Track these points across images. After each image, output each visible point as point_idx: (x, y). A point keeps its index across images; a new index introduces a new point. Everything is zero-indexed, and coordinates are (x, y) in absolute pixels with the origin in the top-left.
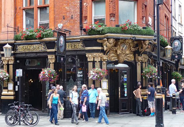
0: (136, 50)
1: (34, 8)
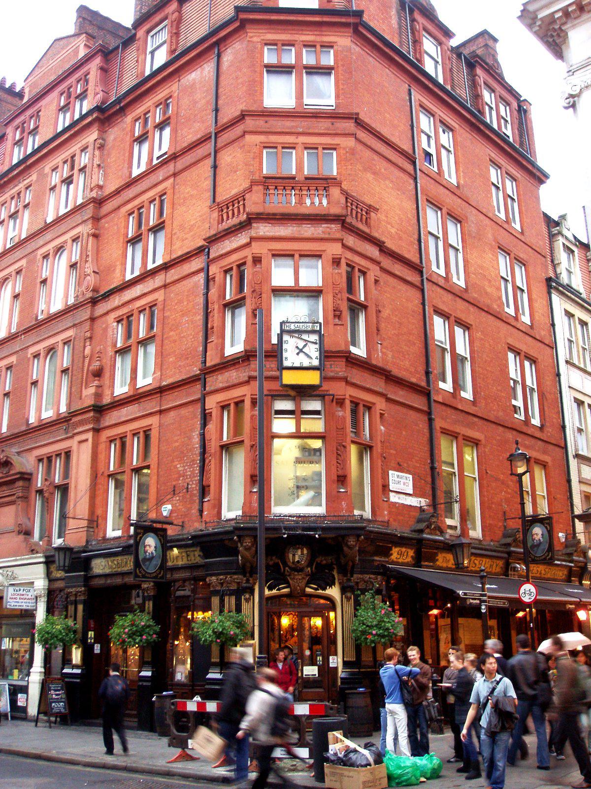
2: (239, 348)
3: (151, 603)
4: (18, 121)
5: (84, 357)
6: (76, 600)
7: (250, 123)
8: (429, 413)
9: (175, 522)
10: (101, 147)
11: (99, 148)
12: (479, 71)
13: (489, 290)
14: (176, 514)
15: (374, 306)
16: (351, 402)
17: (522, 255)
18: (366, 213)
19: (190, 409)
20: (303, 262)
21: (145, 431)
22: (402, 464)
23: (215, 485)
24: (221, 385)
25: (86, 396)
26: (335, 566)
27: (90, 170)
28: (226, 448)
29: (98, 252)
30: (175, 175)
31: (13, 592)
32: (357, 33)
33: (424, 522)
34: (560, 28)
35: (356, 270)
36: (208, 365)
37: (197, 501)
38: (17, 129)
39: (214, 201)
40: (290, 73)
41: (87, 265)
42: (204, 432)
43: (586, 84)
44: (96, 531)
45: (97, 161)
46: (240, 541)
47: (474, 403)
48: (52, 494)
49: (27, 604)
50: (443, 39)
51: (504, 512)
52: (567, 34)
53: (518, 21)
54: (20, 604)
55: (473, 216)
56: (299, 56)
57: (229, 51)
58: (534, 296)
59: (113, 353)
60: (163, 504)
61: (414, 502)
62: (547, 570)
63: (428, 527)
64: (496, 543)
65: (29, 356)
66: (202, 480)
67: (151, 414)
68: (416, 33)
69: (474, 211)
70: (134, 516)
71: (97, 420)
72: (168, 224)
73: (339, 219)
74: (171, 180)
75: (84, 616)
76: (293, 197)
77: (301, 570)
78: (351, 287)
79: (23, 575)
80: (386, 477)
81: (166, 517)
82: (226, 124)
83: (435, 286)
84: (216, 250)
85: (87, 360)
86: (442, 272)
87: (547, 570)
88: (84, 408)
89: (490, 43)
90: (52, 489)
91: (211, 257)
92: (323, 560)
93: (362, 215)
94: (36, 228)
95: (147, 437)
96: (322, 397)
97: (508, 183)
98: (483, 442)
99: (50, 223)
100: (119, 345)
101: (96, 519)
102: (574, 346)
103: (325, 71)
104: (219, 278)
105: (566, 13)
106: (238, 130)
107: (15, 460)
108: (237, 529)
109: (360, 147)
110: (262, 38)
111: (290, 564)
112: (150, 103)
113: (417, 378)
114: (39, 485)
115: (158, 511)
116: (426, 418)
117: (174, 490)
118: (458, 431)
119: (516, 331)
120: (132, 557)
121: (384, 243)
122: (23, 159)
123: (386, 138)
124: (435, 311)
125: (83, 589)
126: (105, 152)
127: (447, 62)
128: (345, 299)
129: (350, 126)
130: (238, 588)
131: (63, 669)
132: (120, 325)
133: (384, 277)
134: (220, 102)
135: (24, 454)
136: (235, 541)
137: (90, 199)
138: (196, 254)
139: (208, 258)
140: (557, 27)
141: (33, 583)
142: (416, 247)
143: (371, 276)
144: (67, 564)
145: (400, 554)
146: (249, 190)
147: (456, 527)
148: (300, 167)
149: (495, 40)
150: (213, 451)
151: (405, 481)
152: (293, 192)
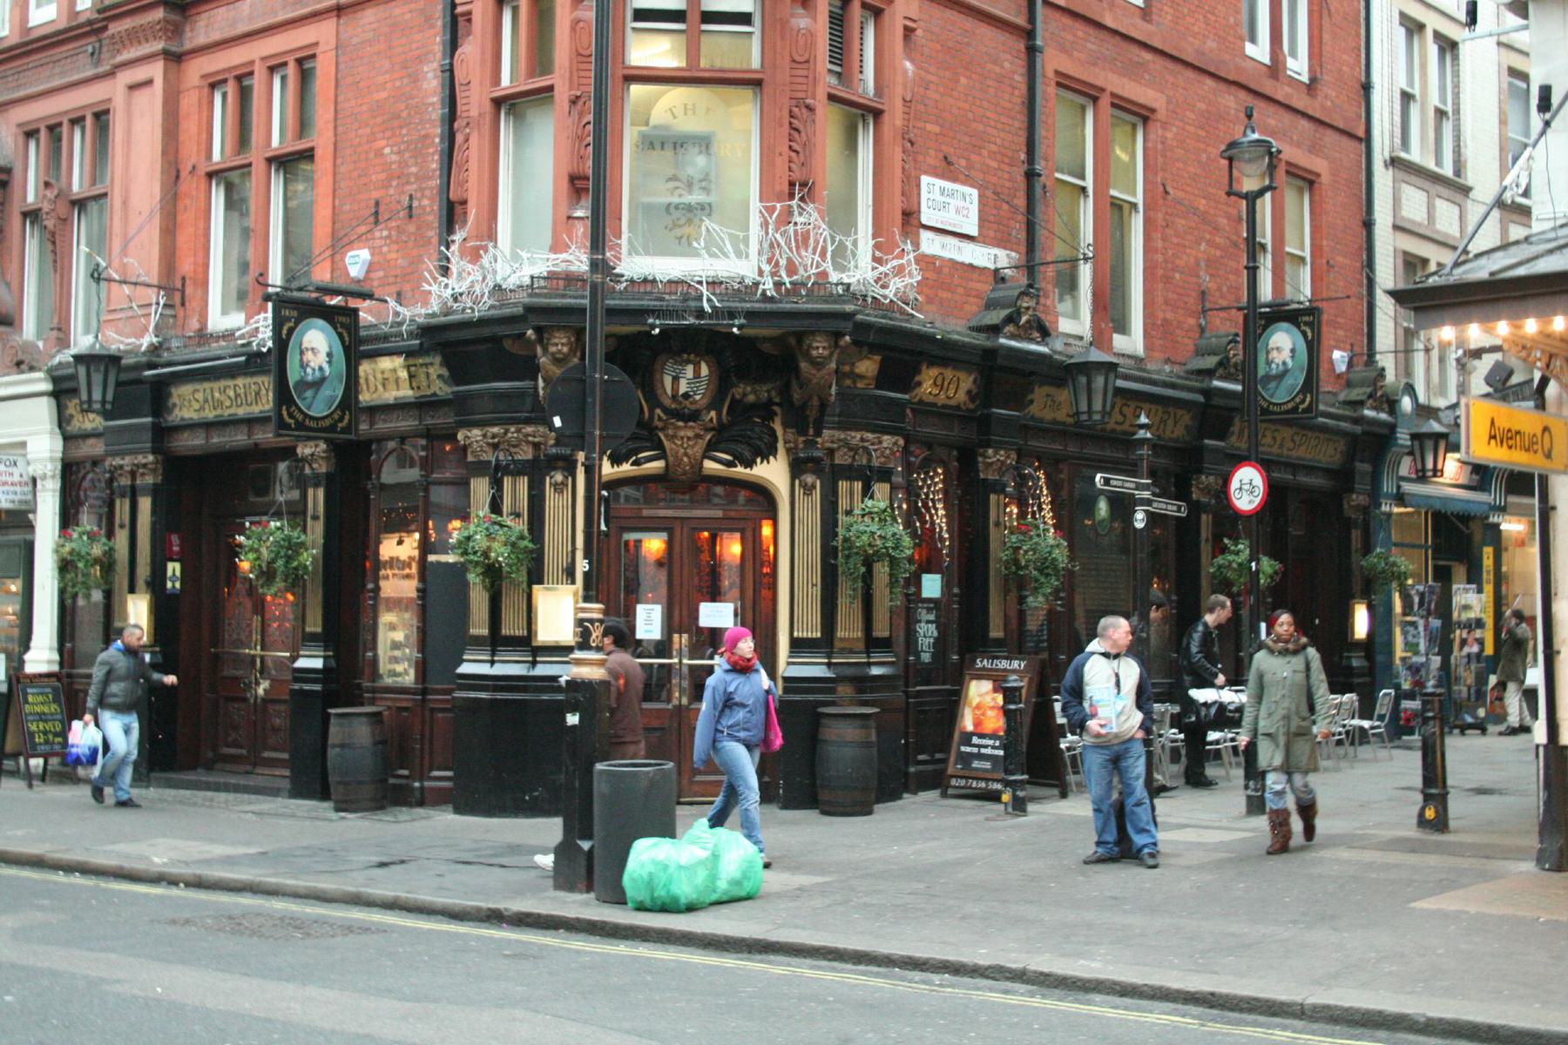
1: (250, 165)
3: (321, 493)
8: (1030, 34)
14: (381, 274)
21: (300, 61)
22: (953, 159)
26: (776, 408)
28: (508, 104)
33: (1003, 307)
42: (451, 65)
44: (181, 313)
46: (540, 340)
48: (65, 221)
49: (12, 497)
60: (350, 245)
62: (1297, 438)
63: (1010, 319)
64: (1176, 369)
67: (315, 16)
70: (276, 277)
75: (154, 525)
77: (694, 416)
80: (911, 189)
87: (1297, 438)
90: (62, 210)
92: (748, 392)
95: (305, 76)
98: (1161, 114)
102: (1414, 110)
108: (530, 310)
111: (667, 402)
114: (31, 198)
115: (337, 266)
117: (377, 213)
118: (1099, 82)
120: (271, 378)
125: (151, 458)
136: (529, 340)
141: (23, 445)
144: (110, 397)
145: (939, 384)
150: (474, 113)
151: (961, 203)
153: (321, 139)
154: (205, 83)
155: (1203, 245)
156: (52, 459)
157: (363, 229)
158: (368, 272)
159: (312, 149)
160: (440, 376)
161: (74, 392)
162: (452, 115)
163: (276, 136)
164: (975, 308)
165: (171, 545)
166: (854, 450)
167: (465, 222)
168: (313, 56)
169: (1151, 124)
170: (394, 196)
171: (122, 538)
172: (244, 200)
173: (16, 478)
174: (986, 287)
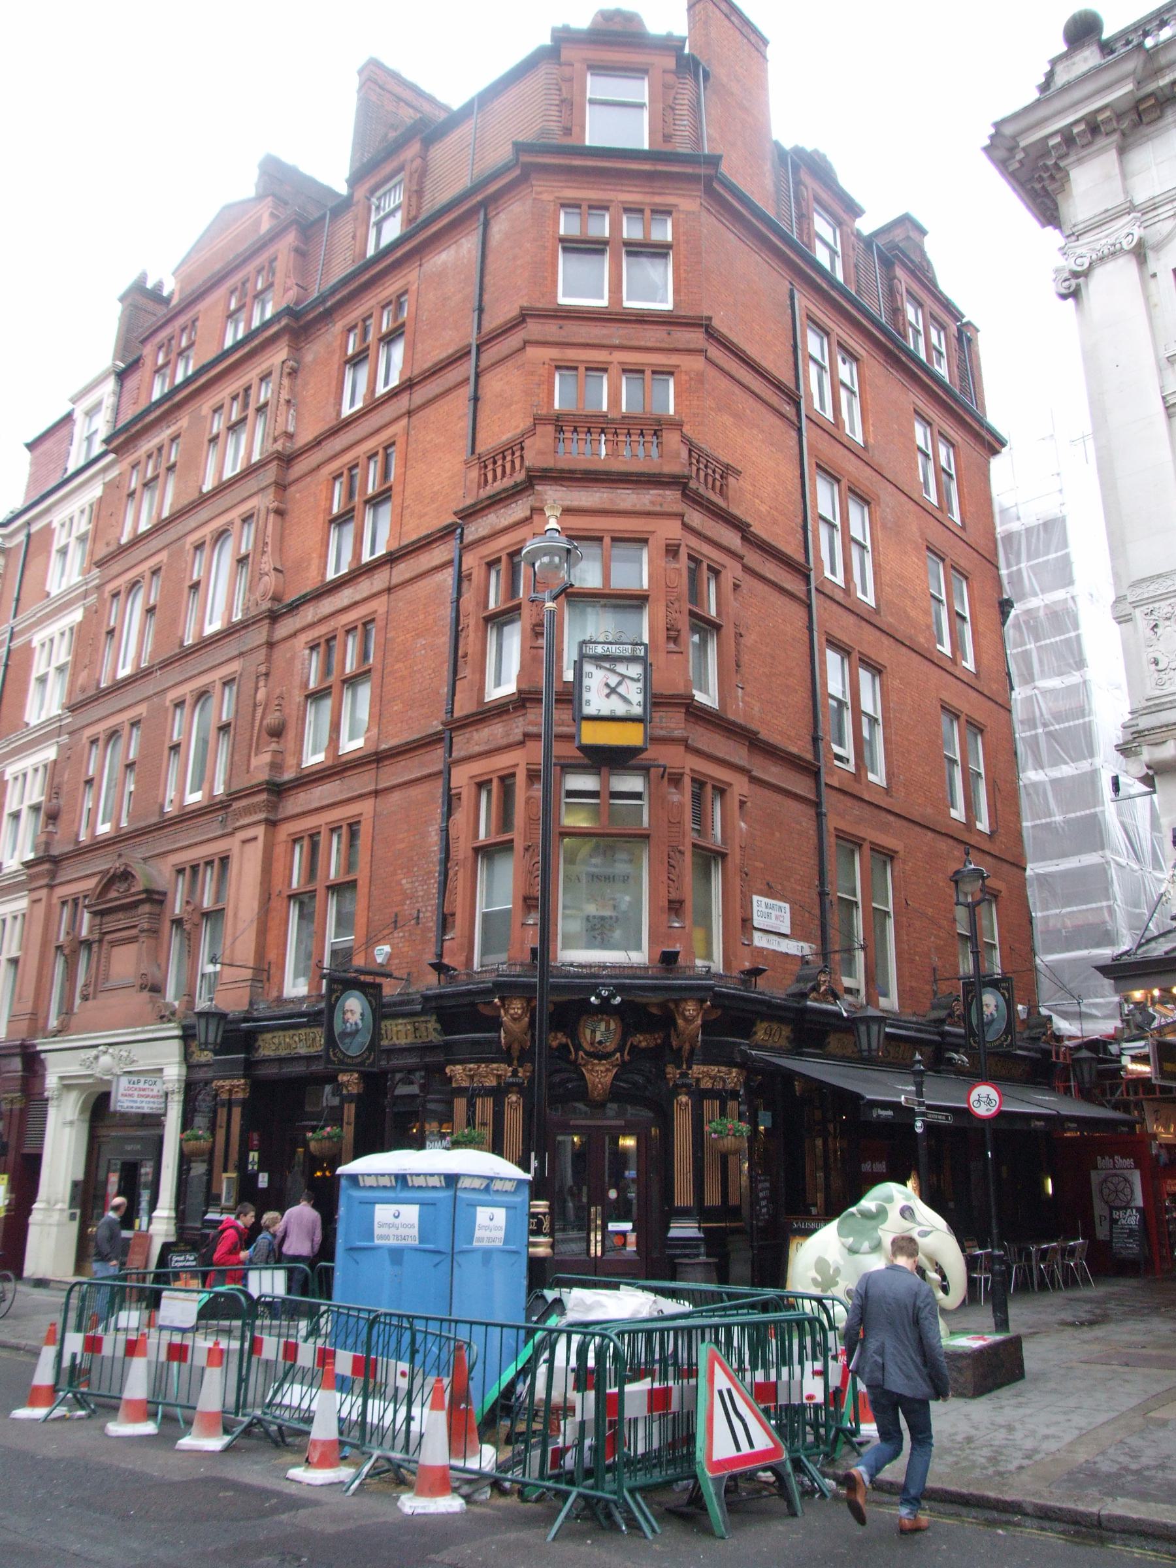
0: (659, 1041)
1: (315, 891)
2: (509, 688)
3: (353, 1106)
4: (163, 335)
5: (255, 706)
6: (230, 1100)
7: (533, 328)
8: (817, 805)
9: (396, 974)
10: (293, 373)
11: (290, 374)
12: (899, 272)
13: (912, 614)
14: (397, 961)
15: (732, 626)
16: (694, 780)
17: (962, 563)
18: (722, 477)
19: (426, 787)
20: (620, 551)
21: (350, 825)
23: (464, 888)
24: (477, 749)
25: (256, 768)
27: (274, 409)
28: (487, 852)
29: (282, 538)
30: (410, 413)
31: (127, 1085)
32: (710, 192)
34: (1056, 164)
35: (705, 566)
36: (456, 715)
37: (434, 939)
38: (160, 348)
39: (473, 452)
40: (601, 252)
41: (265, 559)
43: (1100, 254)
44: (266, 986)
45: (285, 395)
46: (503, 1005)
47: (887, 791)
48: (197, 926)
49: (151, 1105)
50: (845, 217)
51: (934, 969)
52: (1068, 175)
53: (983, 158)
54: (138, 1105)
55: (887, 495)
56: (616, 226)
57: (502, 216)
58: (981, 628)
59: (302, 698)
60: (378, 942)
61: (792, 947)
63: (815, 989)
65: (168, 703)
66: (442, 905)
67: (361, 797)
68: (803, 204)
69: (891, 488)
71: (273, 807)
72: (397, 490)
73: (678, 482)
74: (404, 421)
76: (603, 447)
77: (606, 1056)
78: (695, 593)
79: (144, 1056)
80: (747, 906)
81: (381, 965)
82: (493, 330)
83: (829, 602)
84: (475, 530)
85: (260, 711)
86: (839, 580)
88: (252, 787)
89: (913, 234)
91: (466, 541)
92: (642, 1040)
93: (714, 480)
94: (185, 501)
95: (353, 835)
96: (645, 770)
97: (943, 450)
98: (902, 853)
99: (208, 493)
100: (312, 685)
101: (266, 967)
103: (658, 251)
104: (478, 574)
105: (1068, 139)
106: (513, 341)
107: (137, 870)
109: (712, 373)
110: (557, 194)
112: (373, 302)
113: (799, 747)
114: (177, 911)
115: (369, 955)
116: (811, 812)
117: (396, 922)
119: (954, 680)
121: (749, 526)
122: (167, 394)
123: (755, 362)
124: (827, 640)
126: (299, 381)
127: (851, 253)
128: (687, 612)
129: (696, 338)
130: (499, 1084)
131: (206, 1213)
132: (315, 655)
133: (748, 582)
134: (486, 297)
135: (152, 862)
137: (272, 454)
138: (441, 538)
139: (461, 542)
140: (1050, 162)
141: (161, 1070)
142: (800, 537)
143: (728, 577)
144: (219, 1040)
146: (531, 432)
147: (858, 990)
148: (615, 400)
149: (924, 233)
150: (461, 856)
151: (778, 913)
152: (603, 438)
153: (361, 874)
154: (290, 839)
155: (933, 939)
156: (179, 1080)
157: (386, 932)
158: (389, 959)
159: (355, 881)
160: (435, 1029)
161: (194, 1036)
162: (447, 858)
163: (333, 871)
164: (789, 982)
165: (252, 1140)
166: (714, 1078)
167: (454, 927)
168: (359, 822)
169: (896, 862)
170: (408, 909)
171: (221, 1134)
172: (312, 914)
173: (155, 1093)
174: (796, 968)
